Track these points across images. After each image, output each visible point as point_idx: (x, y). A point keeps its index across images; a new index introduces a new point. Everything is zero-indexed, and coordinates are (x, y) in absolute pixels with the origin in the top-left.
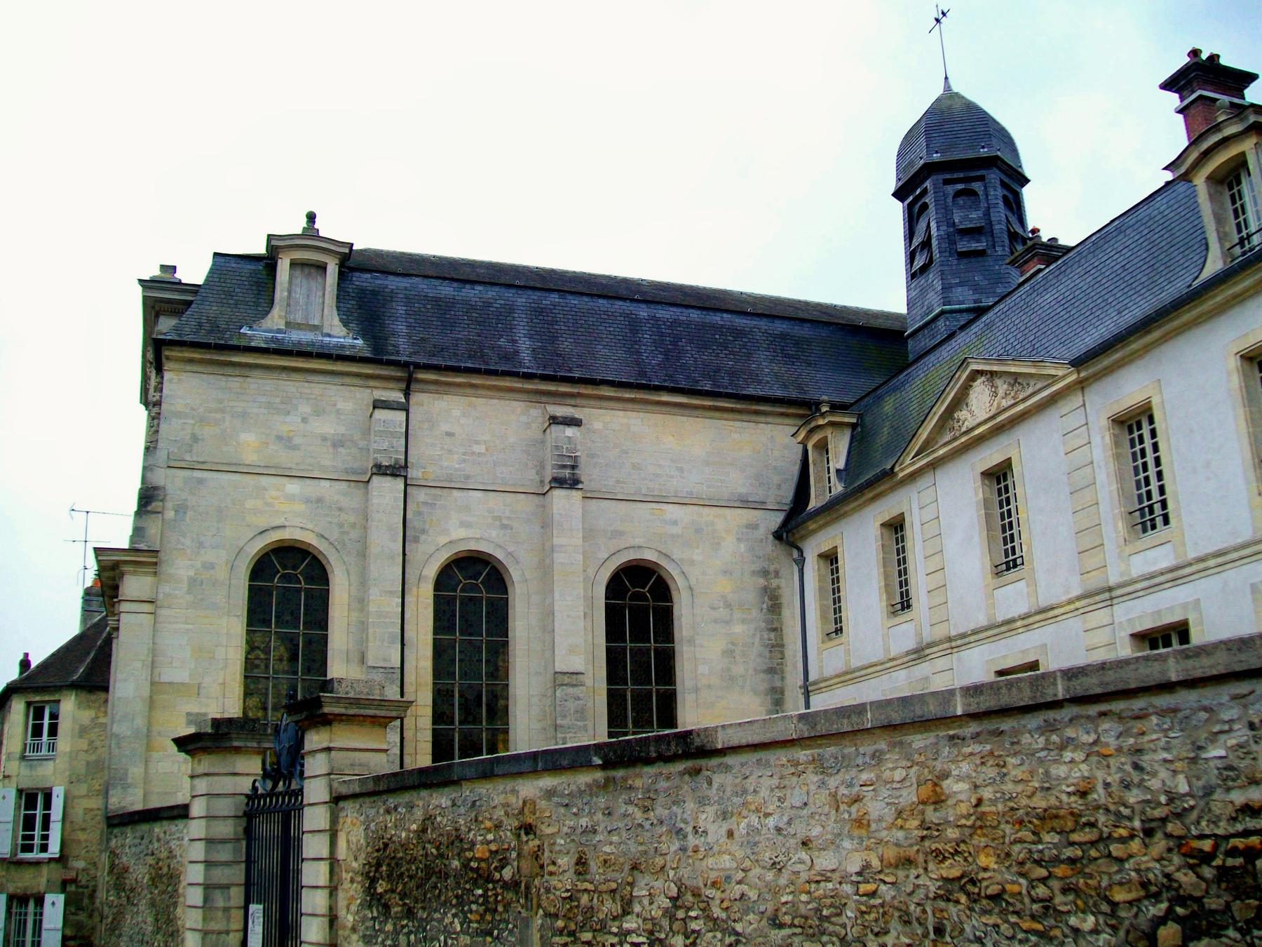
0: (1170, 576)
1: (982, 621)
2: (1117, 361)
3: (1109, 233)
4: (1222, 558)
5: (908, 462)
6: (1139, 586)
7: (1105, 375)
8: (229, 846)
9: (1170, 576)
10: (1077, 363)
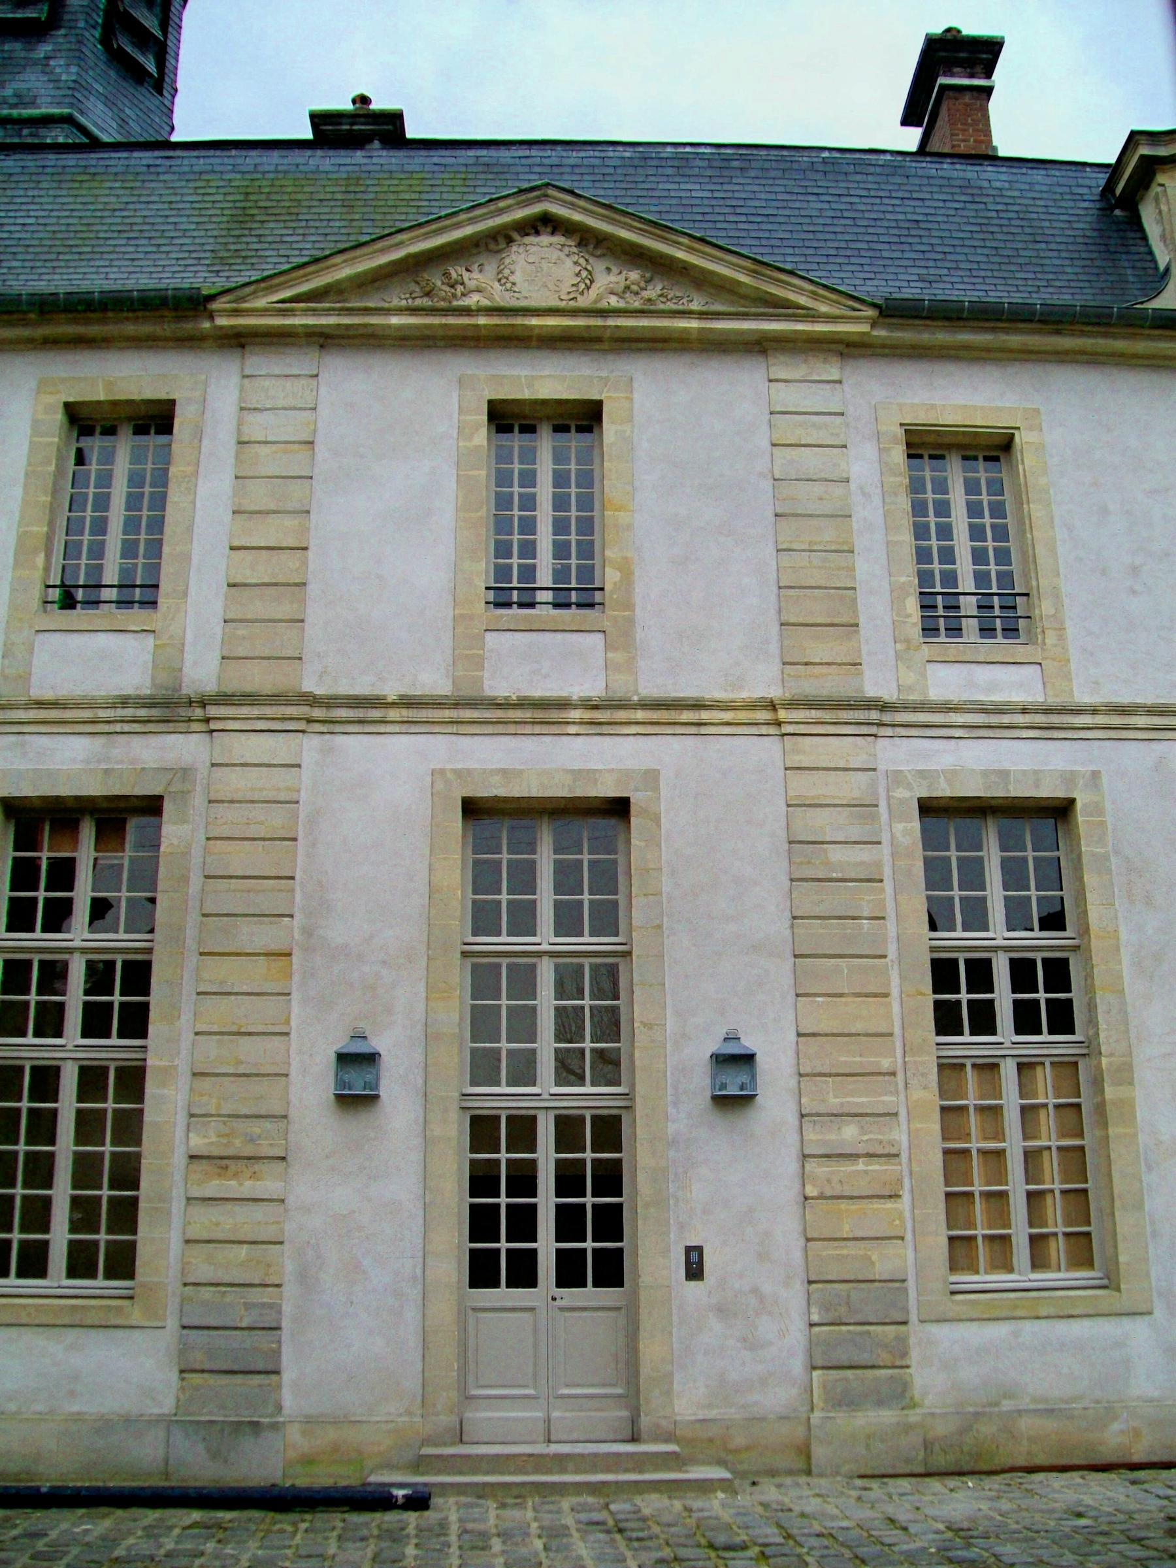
0: (1040, 719)
1: (433, 680)
2: (967, 347)
3: (862, 163)
4: (1121, 719)
5: (261, 303)
6: (959, 718)
7: (910, 357)
8: (538, 600)
9: (1040, 719)
10: (892, 311)
